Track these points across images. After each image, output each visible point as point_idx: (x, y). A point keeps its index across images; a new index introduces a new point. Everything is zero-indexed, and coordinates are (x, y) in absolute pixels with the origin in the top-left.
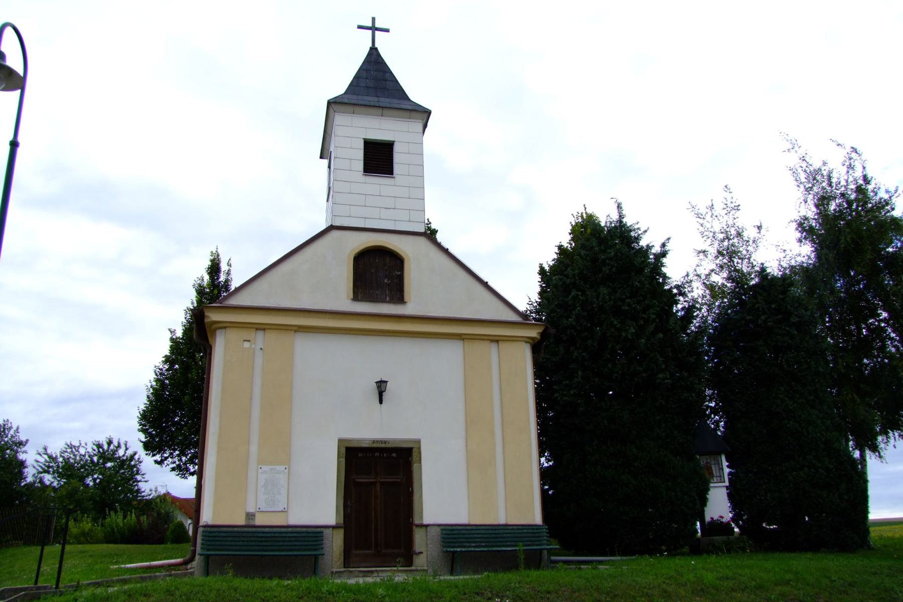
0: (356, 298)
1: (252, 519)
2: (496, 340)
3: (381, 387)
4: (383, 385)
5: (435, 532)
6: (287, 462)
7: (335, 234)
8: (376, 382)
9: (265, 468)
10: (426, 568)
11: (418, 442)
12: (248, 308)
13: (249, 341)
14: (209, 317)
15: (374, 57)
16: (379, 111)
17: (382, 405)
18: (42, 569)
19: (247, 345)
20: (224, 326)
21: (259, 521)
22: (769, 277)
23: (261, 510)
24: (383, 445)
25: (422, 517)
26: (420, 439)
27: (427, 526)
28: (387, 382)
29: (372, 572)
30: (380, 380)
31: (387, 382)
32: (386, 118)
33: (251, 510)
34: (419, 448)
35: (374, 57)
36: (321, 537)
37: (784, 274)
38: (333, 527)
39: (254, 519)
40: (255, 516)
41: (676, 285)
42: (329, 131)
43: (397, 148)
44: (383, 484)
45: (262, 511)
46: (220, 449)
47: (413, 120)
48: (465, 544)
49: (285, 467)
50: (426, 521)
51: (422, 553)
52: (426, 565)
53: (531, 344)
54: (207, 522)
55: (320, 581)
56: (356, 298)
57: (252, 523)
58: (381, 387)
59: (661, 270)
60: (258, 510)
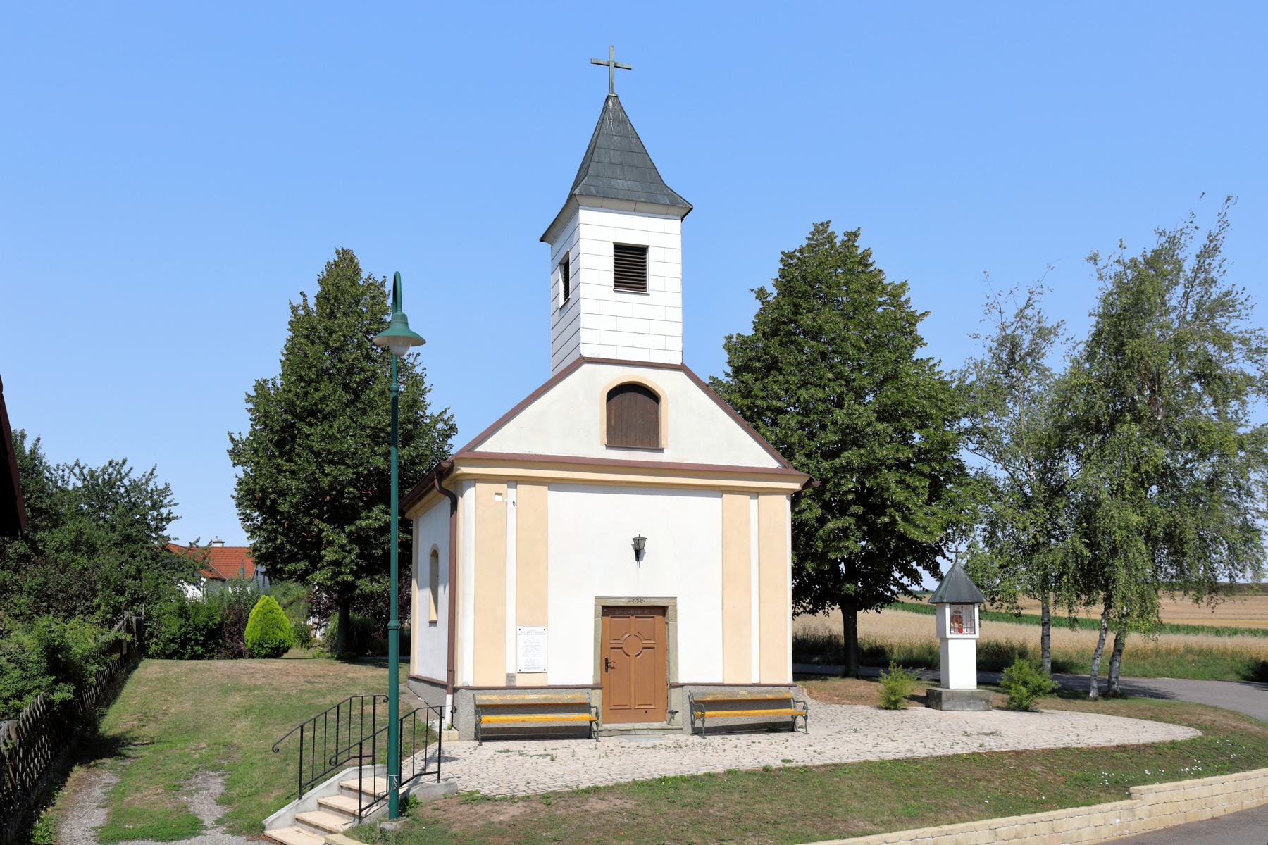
0: (610, 445)
2: (755, 493)
4: (642, 542)
9: (524, 629)
12: (510, 460)
13: (501, 494)
16: (632, 205)
18: (304, 734)
19: (498, 498)
20: (476, 479)
25: (677, 676)
27: (682, 686)
28: (645, 539)
31: (645, 539)
33: (511, 670)
37: (33, 828)
38: (593, 688)
39: (514, 681)
40: (515, 677)
41: (346, 392)
42: (554, 230)
43: (651, 256)
46: (476, 610)
50: (681, 680)
51: (677, 712)
52: (681, 723)
56: (610, 445)
57: (512, 684)
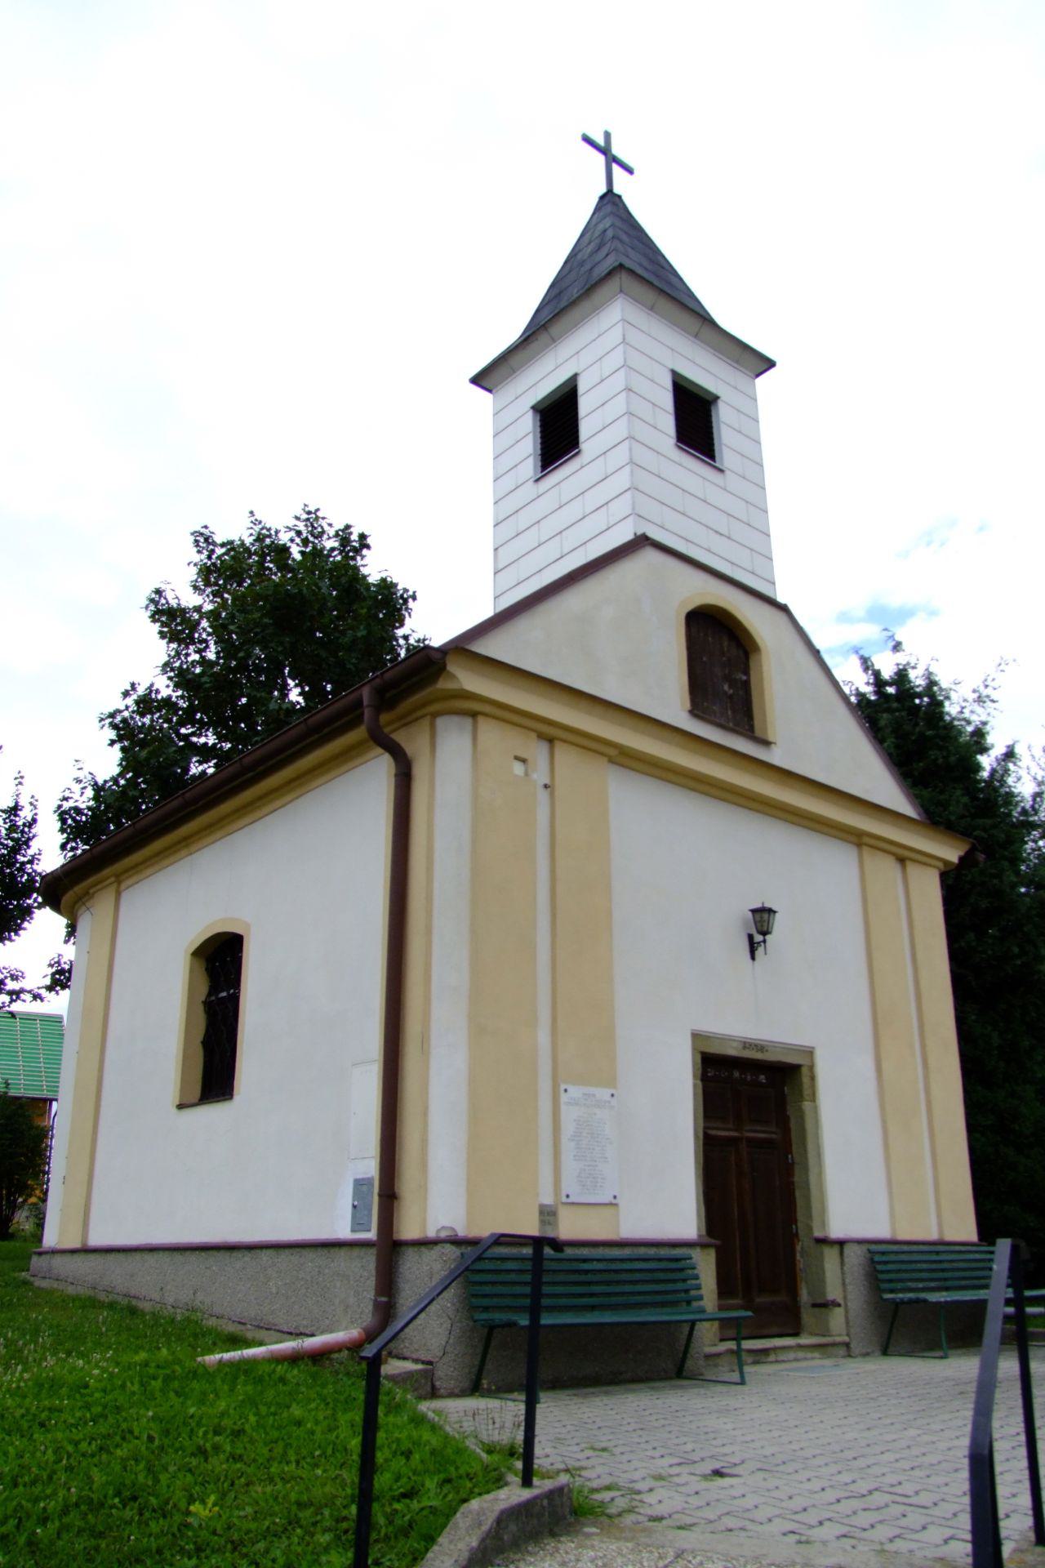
1: (550, 1224)
3: (762, 918)
5: (854, 1255)
6: (611, 1081)
7: (650, 556)
8: (754, 911)
10: (846, 1339)
11: (810, 1053)
14: (453, 677)
15: (610, 201)
17: (755, 962)
19: (518, 769)
21: (569, 1228)
22: (297, 681)
23: (570, 1200)
24: (759, 1056)
25: (823, 1224)
26: (813, 1048)
27: (841, 1243)
29: (765, 1352)
30: (759, 905)
31: (775, 912)
32: (699, 343)
33: (548, 1199)
34: (812, 1068)
35: (610, 201)
36: (987, 1281)
44: (749, 1140)
45: (573, 1203)
47: (743, 370)
48: (910, 1284)
49: (562, 1092)
50: (836, 1230)
53: (940, 870)
54: (452, 1229)
55: (325, 1391)
58: (762, 918)
59: (976, 759)
60: (564, 1199)
